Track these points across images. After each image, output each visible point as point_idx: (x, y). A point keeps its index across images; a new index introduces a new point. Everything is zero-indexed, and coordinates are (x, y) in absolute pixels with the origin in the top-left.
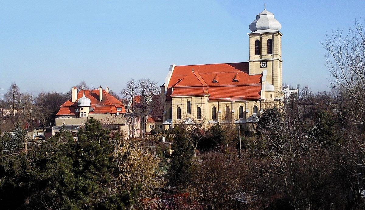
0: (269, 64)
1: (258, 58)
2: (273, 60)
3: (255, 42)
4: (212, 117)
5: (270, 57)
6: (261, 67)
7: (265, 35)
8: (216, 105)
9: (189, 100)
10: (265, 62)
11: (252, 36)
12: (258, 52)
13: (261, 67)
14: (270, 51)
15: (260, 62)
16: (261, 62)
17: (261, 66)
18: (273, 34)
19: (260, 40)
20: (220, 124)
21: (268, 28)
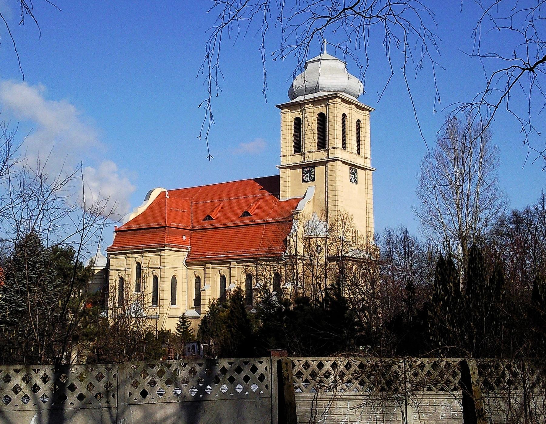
0: (319, 171)
2: (327, 162)
3: (293, 124)
4: (193, 301)
5: (321, 156)
6: (304, 181)
7: (310, 105)
8: (200, 272)
9: (137, 259)
10: (312, 167)
11: (287, 110)
12: (298, 148)
13: (304, 181)
14: (322, 143)
15: (301, 170)
16: (303, 168)
17: (303, 179)
18: (325, 100)
19: (325, 114)
20: (89, 344)
21: (316, 89)
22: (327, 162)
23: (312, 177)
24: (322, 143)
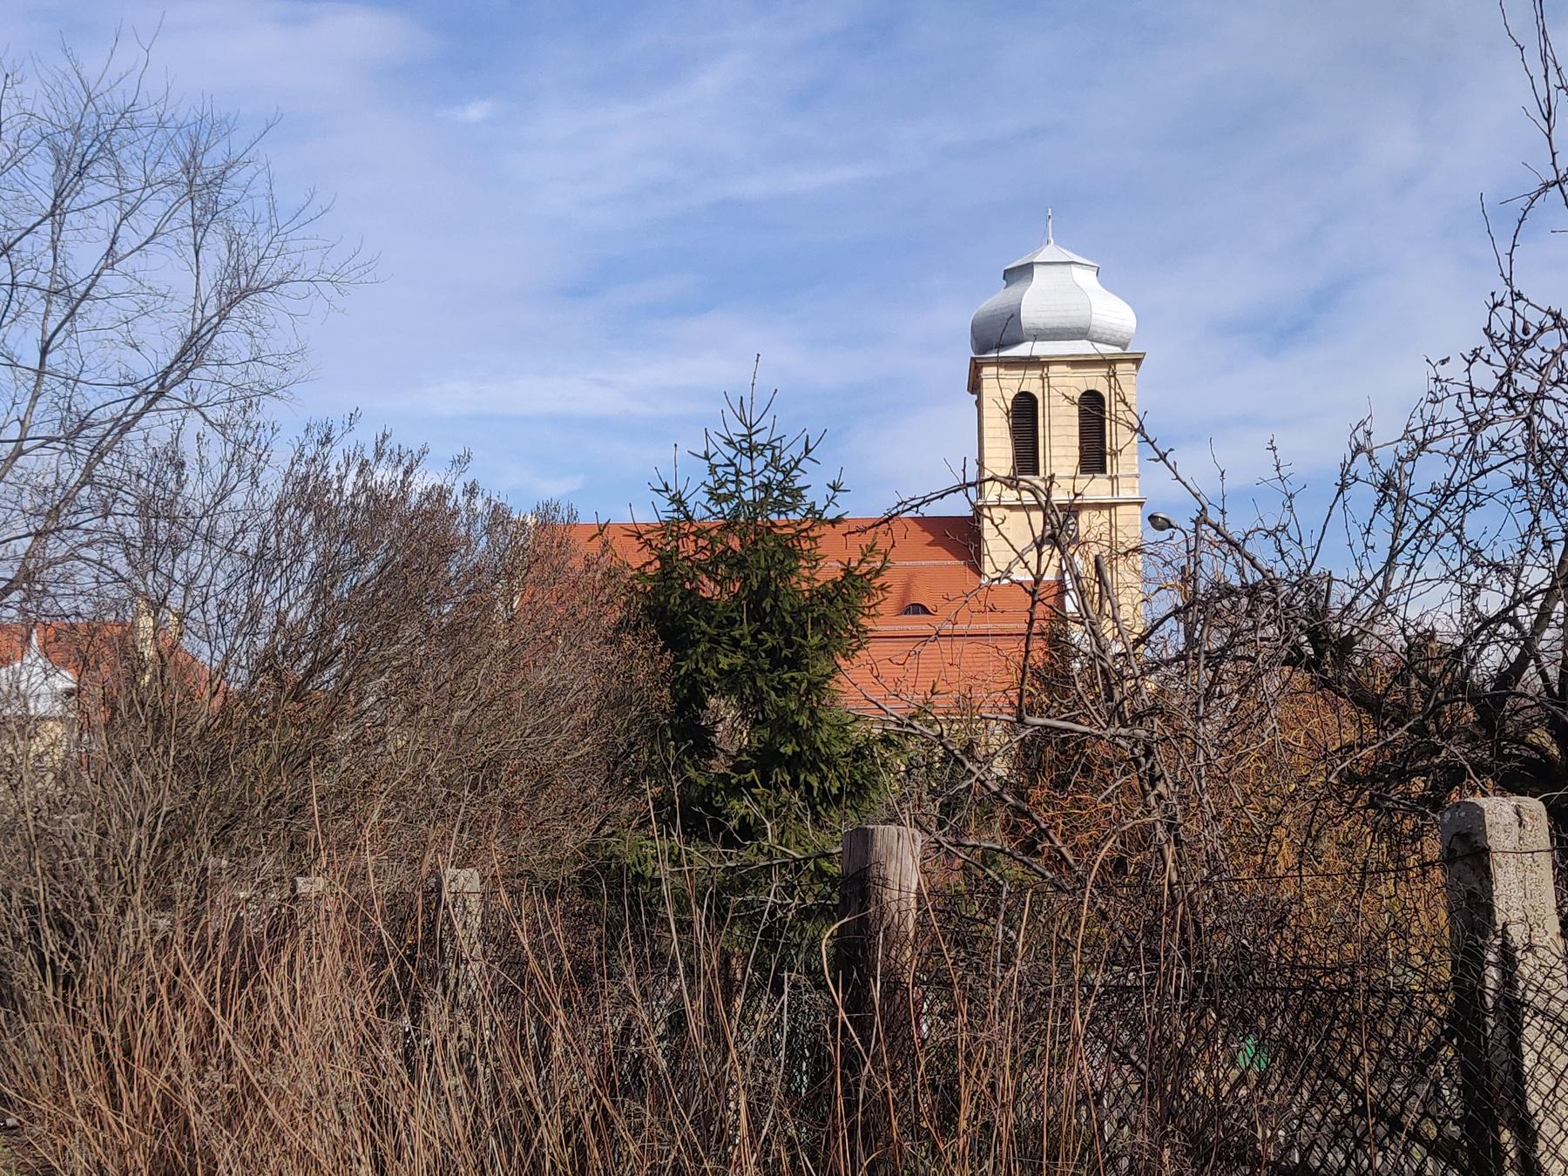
2: (1115, 505)
18: (1108, 362)
22: (1115, 505)
24: (1094, 457)
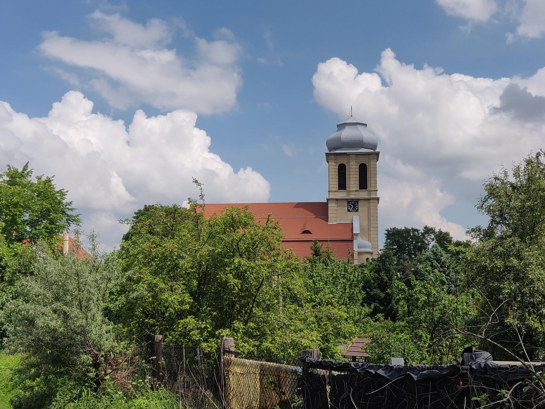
0: (362, 207)
1: (342, 195)
2: (369, 199)
5: (363, 194)
23: (356, 209)
